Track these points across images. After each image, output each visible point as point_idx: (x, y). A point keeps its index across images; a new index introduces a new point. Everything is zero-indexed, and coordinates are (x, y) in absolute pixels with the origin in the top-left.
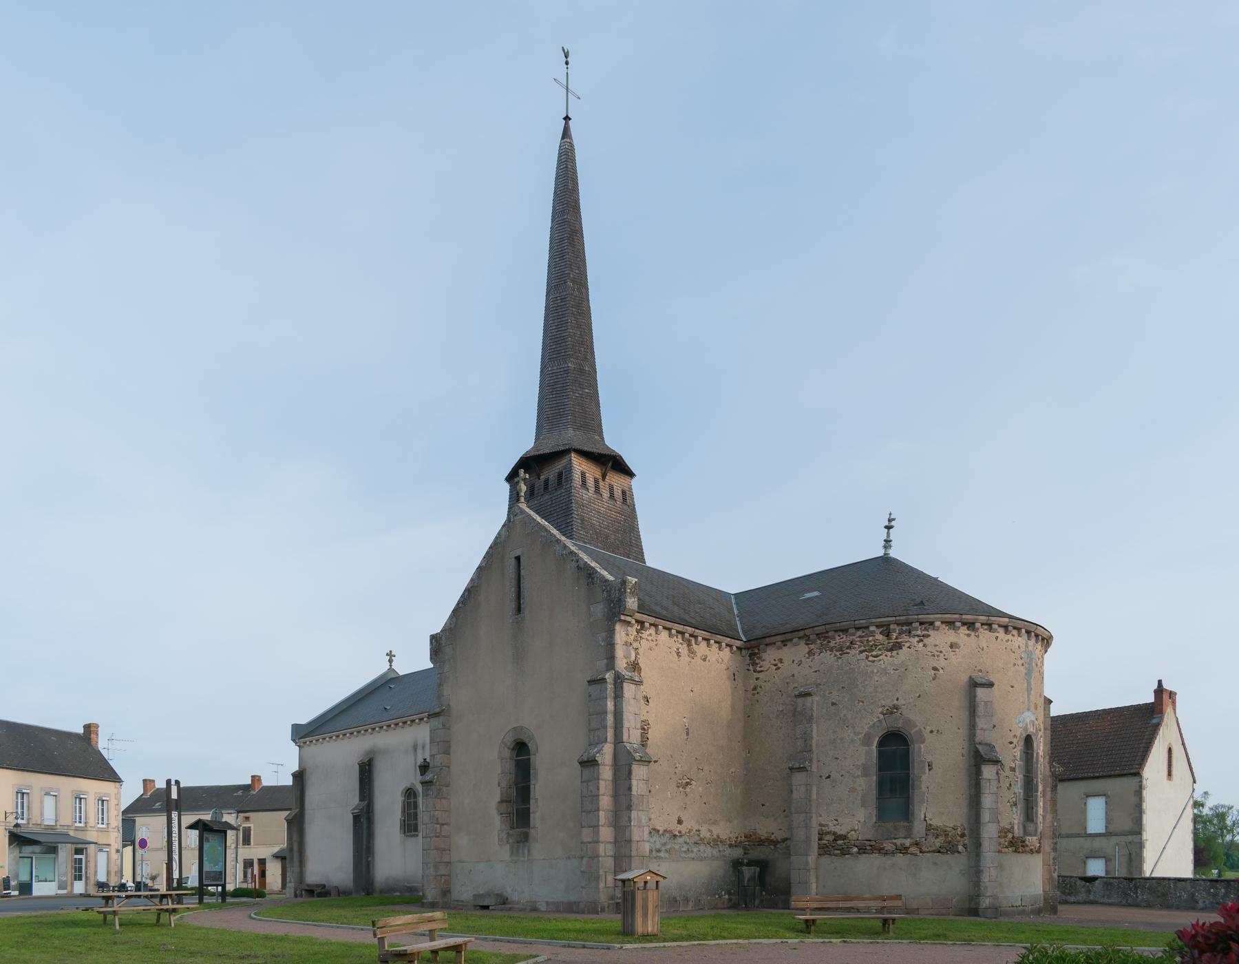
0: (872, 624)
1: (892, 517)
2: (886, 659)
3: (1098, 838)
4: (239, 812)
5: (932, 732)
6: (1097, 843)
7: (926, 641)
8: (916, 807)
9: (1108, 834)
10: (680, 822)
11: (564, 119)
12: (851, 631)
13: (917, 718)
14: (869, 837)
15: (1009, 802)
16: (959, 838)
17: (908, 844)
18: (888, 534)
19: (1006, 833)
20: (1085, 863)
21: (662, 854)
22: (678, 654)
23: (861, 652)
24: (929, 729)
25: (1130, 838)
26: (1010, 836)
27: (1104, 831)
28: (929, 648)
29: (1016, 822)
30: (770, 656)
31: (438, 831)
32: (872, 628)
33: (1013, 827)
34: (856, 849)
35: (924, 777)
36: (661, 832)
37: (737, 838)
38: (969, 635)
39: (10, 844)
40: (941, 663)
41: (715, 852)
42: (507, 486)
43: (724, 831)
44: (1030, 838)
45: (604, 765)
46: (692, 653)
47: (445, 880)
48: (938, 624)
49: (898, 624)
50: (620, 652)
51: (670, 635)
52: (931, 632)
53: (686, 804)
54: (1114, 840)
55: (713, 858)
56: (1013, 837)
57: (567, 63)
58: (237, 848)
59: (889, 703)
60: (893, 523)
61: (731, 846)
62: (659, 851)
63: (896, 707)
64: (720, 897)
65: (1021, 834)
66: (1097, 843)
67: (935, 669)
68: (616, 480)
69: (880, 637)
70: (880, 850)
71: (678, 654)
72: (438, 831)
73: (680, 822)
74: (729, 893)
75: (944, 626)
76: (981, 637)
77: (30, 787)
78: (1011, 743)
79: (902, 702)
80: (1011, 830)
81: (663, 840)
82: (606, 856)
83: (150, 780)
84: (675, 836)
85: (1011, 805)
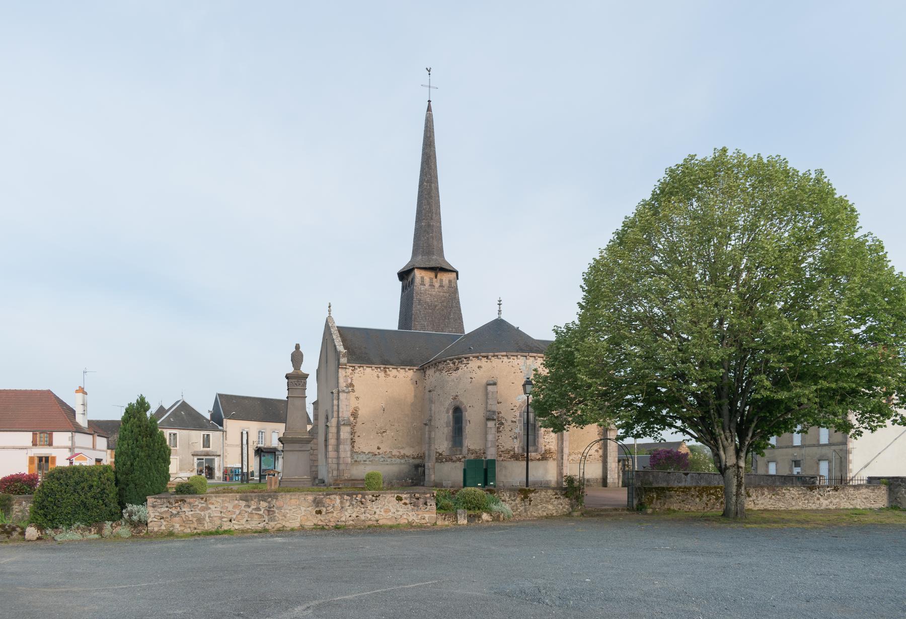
0: (448, 360)
2: (454, 375)
3: (824, 447)
5: (470, 407)
6: (825, 451)
7: (468, 366)
8: (464, 441)
9: (830, 444)
12: (442, 362)
13: (465, 401)
14: (448, 454)
15: (510, 437)
16: (482, 454)
17: (461, 457)
20: (818, 464)
21: (367, 462)
22: (378, 377)
23: (446, 372)
24: (469, 405)
25: (841, 447)
26: (512, 453)
27: (827, 443)
28: (469, 369)
29: (516, 446)
30: (430, 372)
31: (312, 452)
32: (448, 361)
33: (514, 449)
34: (444, 460)
35: (467, 427)
36: (366, 453)
37: (418, 455)
38: (487, 362)
39: (255, 456)
40: (473, 375)
41: (403, 461)
42: (398, 285)
43: (408, 451)
45: (332, 427)
46: (387, 375)
47: (315, 474)
48: (471, 358)
49: (457, 359)
50: (341, 380)
51: (372, 370)
52: (469, 362)
53: (382, 440)
54: (833, 448)
55: (401, 464)
56: (514, 453)
57: (429, 74)
59: (454, 394)
60: (501, 302)
61: (413, 458)
62: (365, 461)
63: (457, 396)
64: (405, 481)
66: (825, 451)
67: (471, 378)
68: (445, 277)
69: (451, 365)
70: (451, 460)
71: (378, 377)
72: (312, 452)
73: (379, 448)
74: (412, 479)
75: (475, 358)
76: (493, 362)
77: (264, 429)
78: (512, 409)
79: (459, 393)
81: (367, 456)
82: (332, 463)
84: (376, 455)
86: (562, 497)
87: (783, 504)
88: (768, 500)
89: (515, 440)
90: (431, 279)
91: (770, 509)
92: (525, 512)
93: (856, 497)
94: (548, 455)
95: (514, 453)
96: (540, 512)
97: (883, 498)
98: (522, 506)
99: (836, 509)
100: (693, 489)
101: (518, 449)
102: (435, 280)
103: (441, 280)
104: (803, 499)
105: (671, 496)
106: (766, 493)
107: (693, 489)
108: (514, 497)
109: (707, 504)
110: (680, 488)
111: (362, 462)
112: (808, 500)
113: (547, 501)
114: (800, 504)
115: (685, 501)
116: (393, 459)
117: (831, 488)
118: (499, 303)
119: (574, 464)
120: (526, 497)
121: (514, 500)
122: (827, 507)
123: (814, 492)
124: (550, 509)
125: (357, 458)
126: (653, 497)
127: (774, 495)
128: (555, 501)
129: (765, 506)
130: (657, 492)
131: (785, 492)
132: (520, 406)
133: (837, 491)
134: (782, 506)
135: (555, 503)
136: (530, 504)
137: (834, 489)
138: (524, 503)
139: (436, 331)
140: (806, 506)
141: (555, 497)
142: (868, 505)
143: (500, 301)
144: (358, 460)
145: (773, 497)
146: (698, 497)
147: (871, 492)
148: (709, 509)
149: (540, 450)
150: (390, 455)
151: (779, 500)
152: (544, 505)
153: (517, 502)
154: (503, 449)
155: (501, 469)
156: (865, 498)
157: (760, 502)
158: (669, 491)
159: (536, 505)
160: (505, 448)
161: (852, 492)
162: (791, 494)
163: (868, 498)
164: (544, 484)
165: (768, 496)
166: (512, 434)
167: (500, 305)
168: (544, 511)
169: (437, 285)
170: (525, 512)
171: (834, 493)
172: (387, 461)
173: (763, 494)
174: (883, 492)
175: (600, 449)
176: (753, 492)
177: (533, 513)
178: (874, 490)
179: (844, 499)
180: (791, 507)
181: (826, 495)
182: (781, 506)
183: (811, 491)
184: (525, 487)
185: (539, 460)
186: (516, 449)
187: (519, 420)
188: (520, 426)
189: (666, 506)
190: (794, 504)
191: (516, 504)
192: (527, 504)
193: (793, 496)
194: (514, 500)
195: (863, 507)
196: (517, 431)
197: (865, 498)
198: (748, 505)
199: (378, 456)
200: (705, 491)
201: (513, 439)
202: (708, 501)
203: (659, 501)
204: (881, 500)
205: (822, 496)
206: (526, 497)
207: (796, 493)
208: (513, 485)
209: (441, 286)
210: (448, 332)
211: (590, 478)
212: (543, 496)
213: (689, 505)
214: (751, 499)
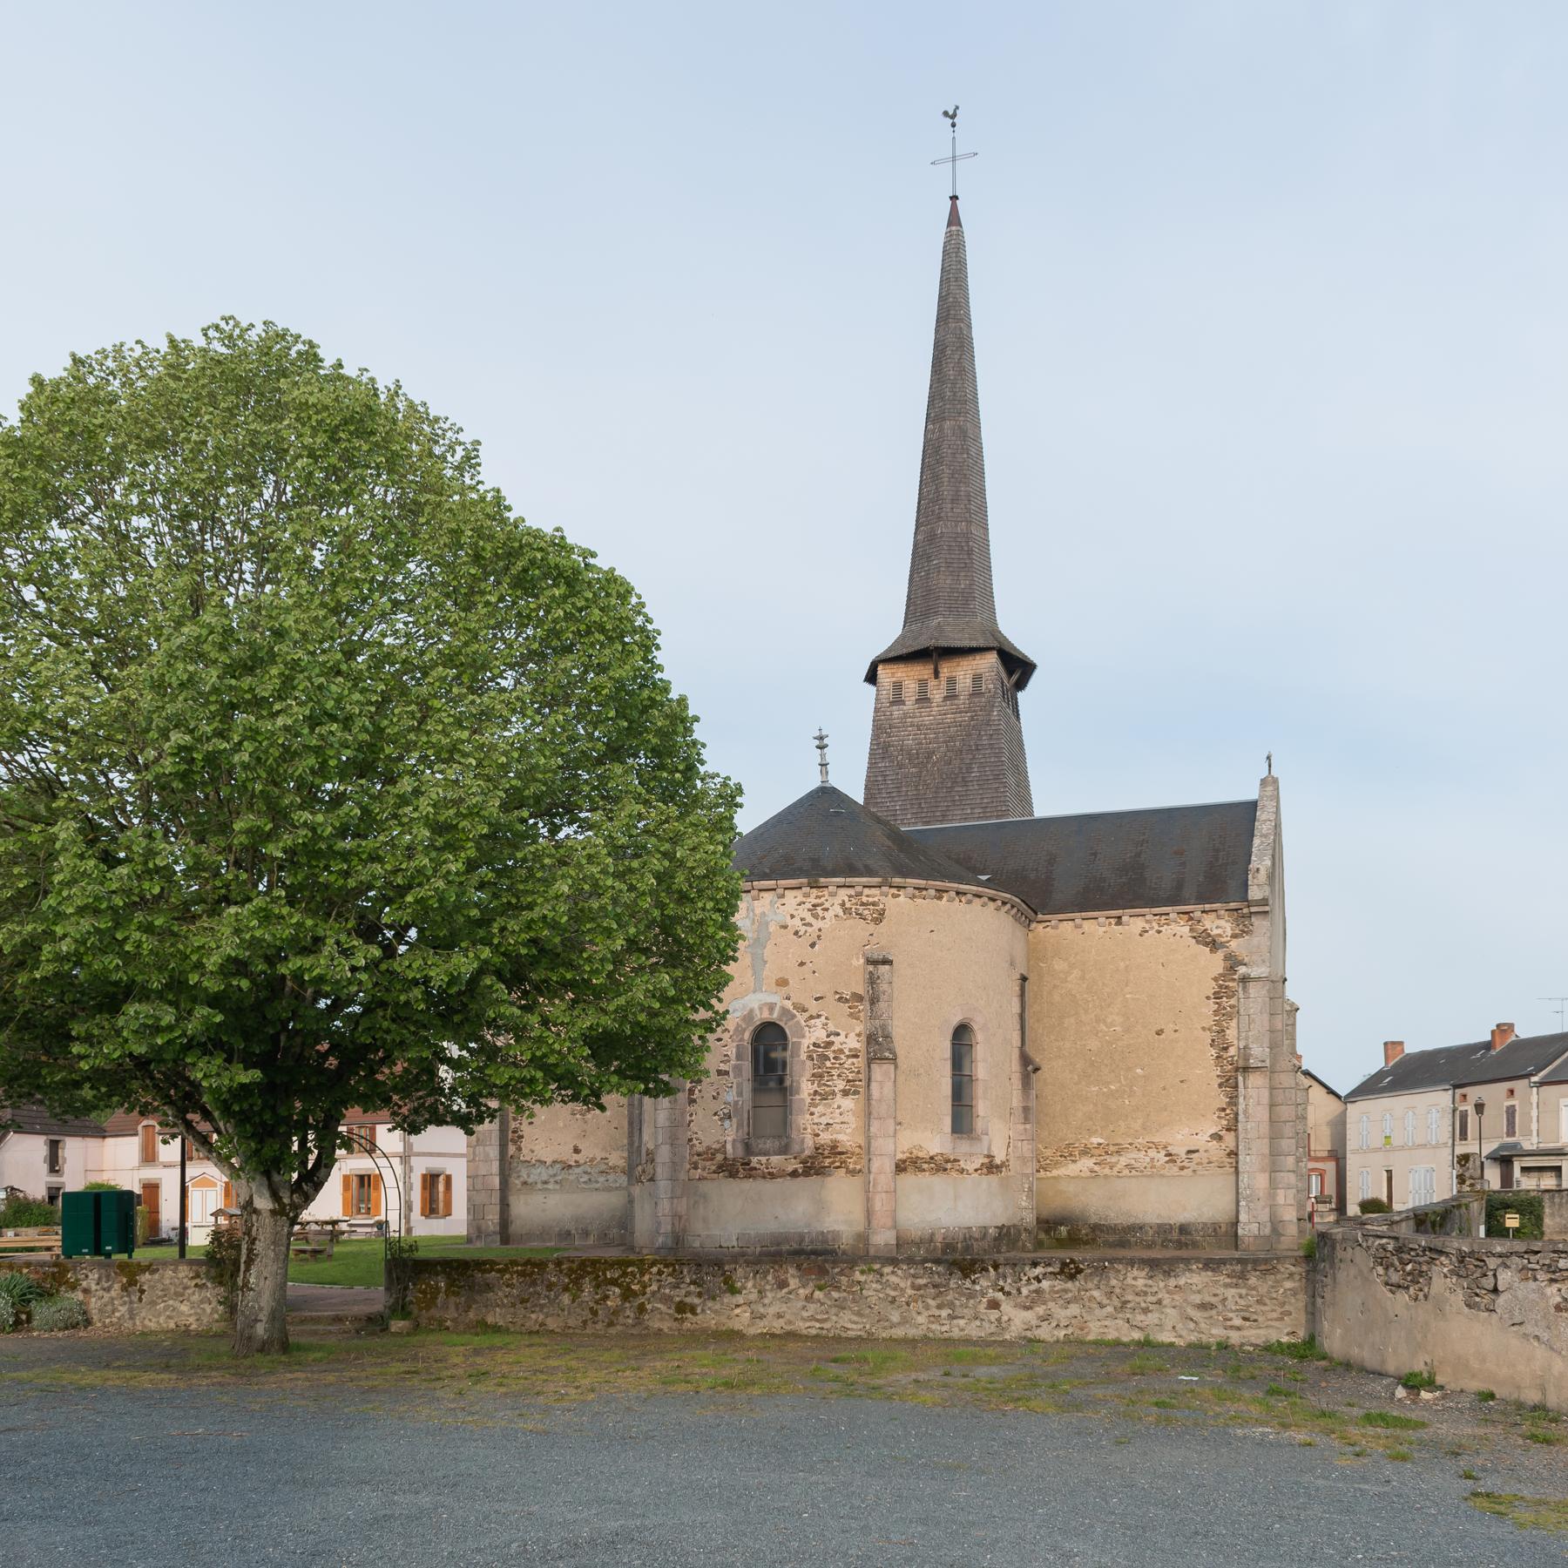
1: (824, 733)
4: (1456, 1087)
10: (577, 1151)
11: (951, 198)
15: (715, 1114)
18: (823, 756)
19: (713, 1154)
21: (550, 1186)
26: (720, 1157)
29: (729, 1139)
33: (724, 1146)
44: (763, 1159)
56: (725, 1159)
58: (1453, 1145)
62: (546, 1182)
65: (740, 1152)
73: (577, 1151)
80: (723, 1149)
83: (1393, 1043)
84: (570, 1166)
85: (721, 1119)
86: (209, 1285)
87: (855, 1318)
88: (800, 1304)
89: (727, 1123)
90: (923, 684)
91: (805, 1332)
92: (131, 1318)
93: (1159, 1302)
94: (828, 1160)
95: (725, 1159)
96: (162, 1320)
97: (1287, 1307)
98: (125, 1303)
99: (1067, 1341)
100: (551, 1266)
101: (733, 1148)
102: (932, 683)
103: (952, 681)
104: (932, 1303)
105: (489, 1287)
106: (793, 1283)
107: (551, 1266)
108: (108, 1281)
109: (594, 1313)
110: (514, 1263)
111: (539, 1186)
112: (951, 1305)
113: (177, 1294)
114: (921, 1319)
115: (527, 1301)
116: (611, 1177)
117: (1050, 1269)
118: (817, 742)
119: (1134, 1180)
120: (132, 1282)
121: (108, 1290)
122: (1029, 1334)
123: (974, 1282)
124: (182, 1313)
125: (529, 1176)
126: (438, 1289)
127: (820, 1289)
128: (194, 1294)
129: (790, 1322)
130: (449, 1276)
131: (862, 1278)
132: (736, 1029)
133: (1072, 1277)
134: (849, 1326)
135: (196, 1298)
136: (140, 1300)
137: (1061, 1272)
138: (129, 1296)
139: (998, 817)
140: (944, 1328)
141: (194, 1282)
142: (1214, 1331)
143: (821, 738)
144: (530, 1181)
145: (818, 1294)
146: (566, 1289)
147: (1227, 1286)
148: (599, 1326)
149: (796, 1148)
150: (603, 1167)
151: (840, 1306)
152: (171, 1302)
153: (113, 1293)
154: (699, 1149)
155: (696, 1202)
156: (1203, 1306)
157: (772, 1310)
158: (485, 1271)
159: (153, 1303)
160: (704, 1145)
161: (1140, 1282)
162: (887, 1284)
163: (1212, 1306)
164: (812, 1242)
165: (801, 1291)
166: (718, 1106)
167: (821, 747)
168: (169, 1317)
169: (937, 694)
170: (131, 1318)
171: (1059, 1284)
172: (597, 1182)
173: (782, 1284)
174: (1288, 1285)
175: (1228, 1130)
176: (747, 1278)
177: (147, 1322)
178: (1243, 1276)
179: (1102, 1306)
180: (885, 1328)
181: (1025, 1291)
182: (850, 1323)
183: (966, 1276)
184: (894, 1254)
185: (794, 1174)
186: (729, 1147)
187: (736, 1067)
188: (739, 1085)
189: (471, 1315)
190: (895, 1318)
191: (112, 1299)
192: (135, 1298)
193: (893, 1293)
194: (108, 1290)
195: (1193, 1338)
196: (731, 1096)
197: (1203, 1306)
198: (729, 1318)
199: (577, 1170)
200: (589, 1273)
201: (721, 1119)
202: (597, 1302)
203: (453, 1299)
204: (1275, 1315)
205: (1008, 1294)
206: (132, 1282)
207: (906, 1284)
208: (723, 1245)
209: (951, 696)
210: (960, 820)
211: (1193, 1220)
212: (168, 1282)
213: (541, 1311)
214: (740, 1299)
